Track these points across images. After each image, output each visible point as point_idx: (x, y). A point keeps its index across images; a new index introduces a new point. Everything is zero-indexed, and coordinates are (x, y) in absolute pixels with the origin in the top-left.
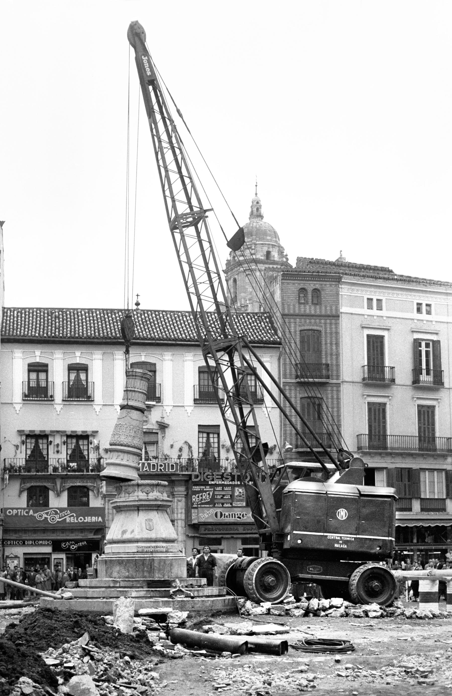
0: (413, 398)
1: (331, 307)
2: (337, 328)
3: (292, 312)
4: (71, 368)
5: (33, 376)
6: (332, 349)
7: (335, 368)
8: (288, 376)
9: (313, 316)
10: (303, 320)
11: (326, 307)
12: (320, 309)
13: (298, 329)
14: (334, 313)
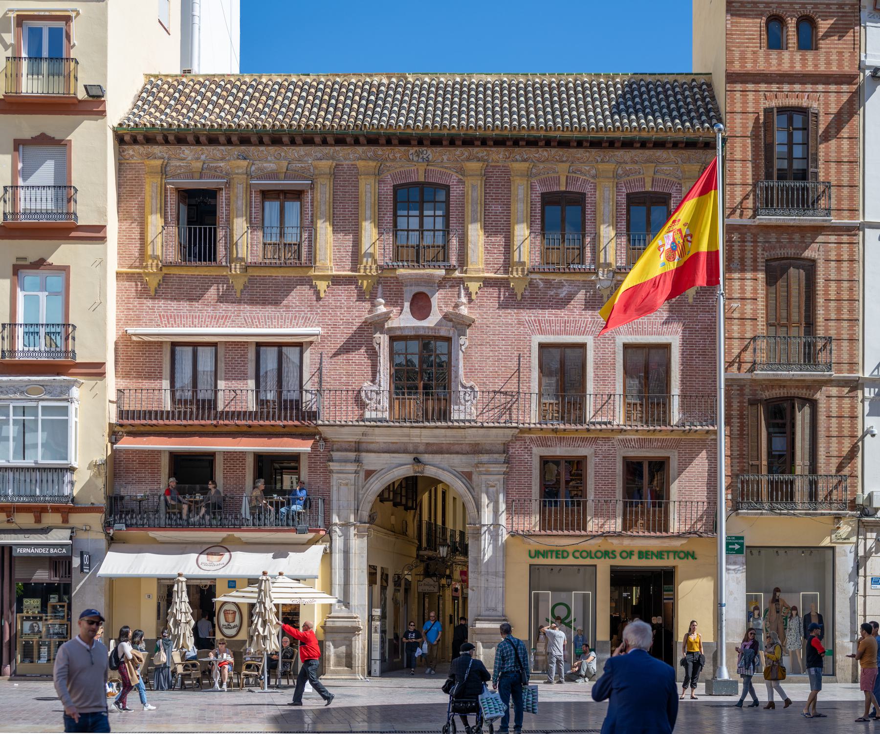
12: (816, 59)
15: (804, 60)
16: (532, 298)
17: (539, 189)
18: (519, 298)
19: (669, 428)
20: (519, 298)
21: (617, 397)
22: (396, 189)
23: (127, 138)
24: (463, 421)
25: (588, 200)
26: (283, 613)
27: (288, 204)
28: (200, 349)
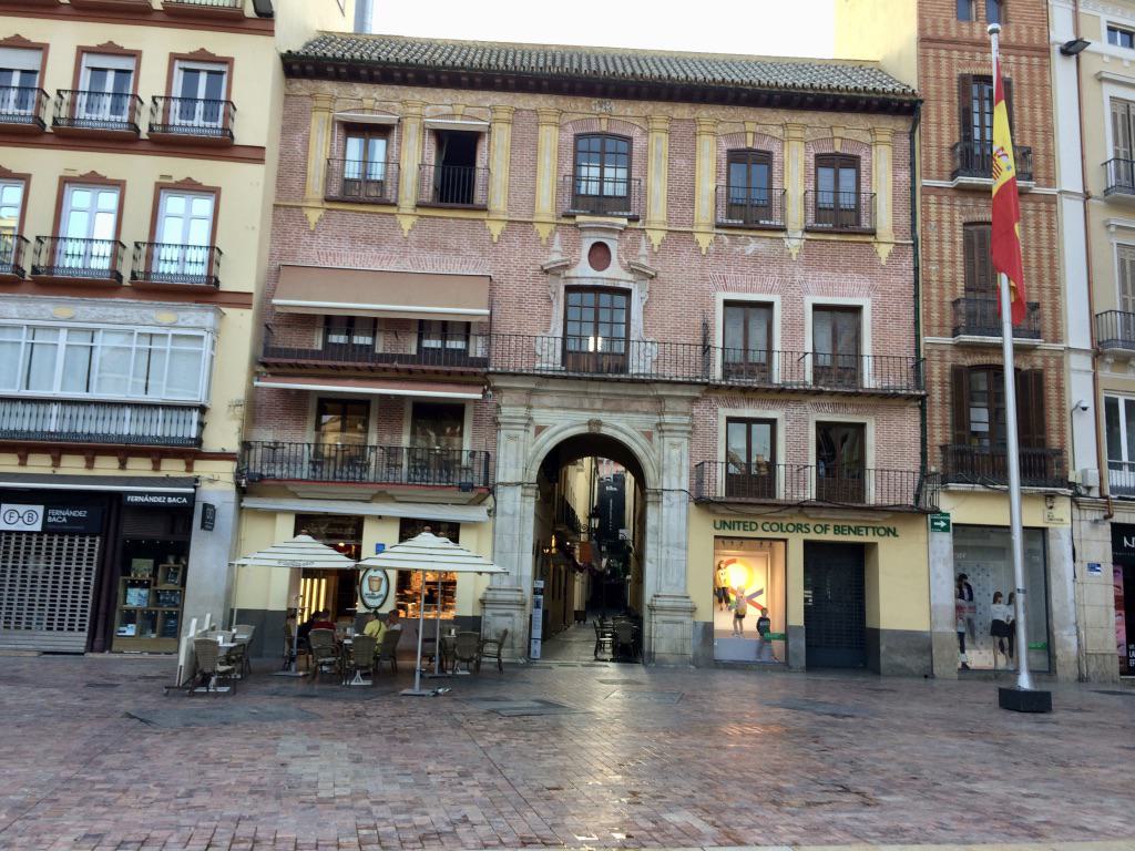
0: (1108, 226)
1: (1030, 29)
2: (1042, 75)
3: (941, 33)
4: (735, 157)
5: (739, 171)
6: (1033, 120)
7: (1041, 160)
8: (934, 173)
9: (940, 40)
10: (955, 52)
11: (1018, 29)
13: (956, 74)
14: (1036, 40)
16: (717, 253)
17: (726, 146)
25: (775, 159)
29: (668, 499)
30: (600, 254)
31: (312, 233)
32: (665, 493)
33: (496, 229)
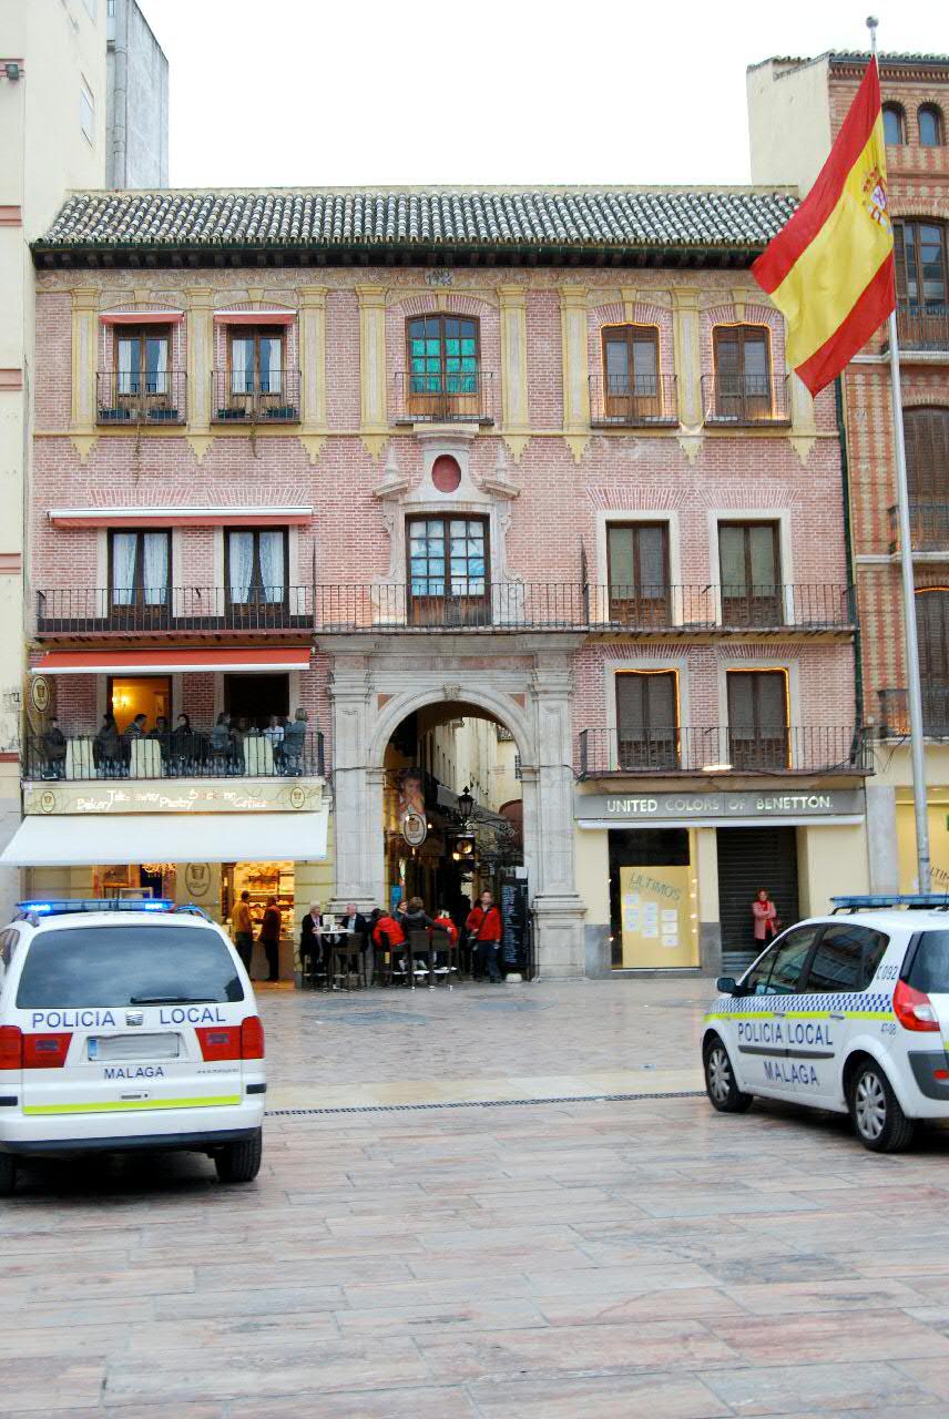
5: (618, 351)
15: (930, 157)
18: (578, 460)
19: (490, 629)
20: (578, 460)
21: (600, 589)
22: (410, 320)
23: (49, 259)
24: (388, 626)
26: (96, 897)
27: (637, 347)
28: (147, 536)
29: (548, 776)
30: (447, 468)
31: (83, 467)
32: (543, 771)
33: (314, 447)
